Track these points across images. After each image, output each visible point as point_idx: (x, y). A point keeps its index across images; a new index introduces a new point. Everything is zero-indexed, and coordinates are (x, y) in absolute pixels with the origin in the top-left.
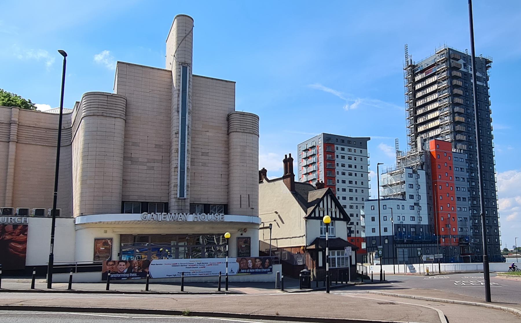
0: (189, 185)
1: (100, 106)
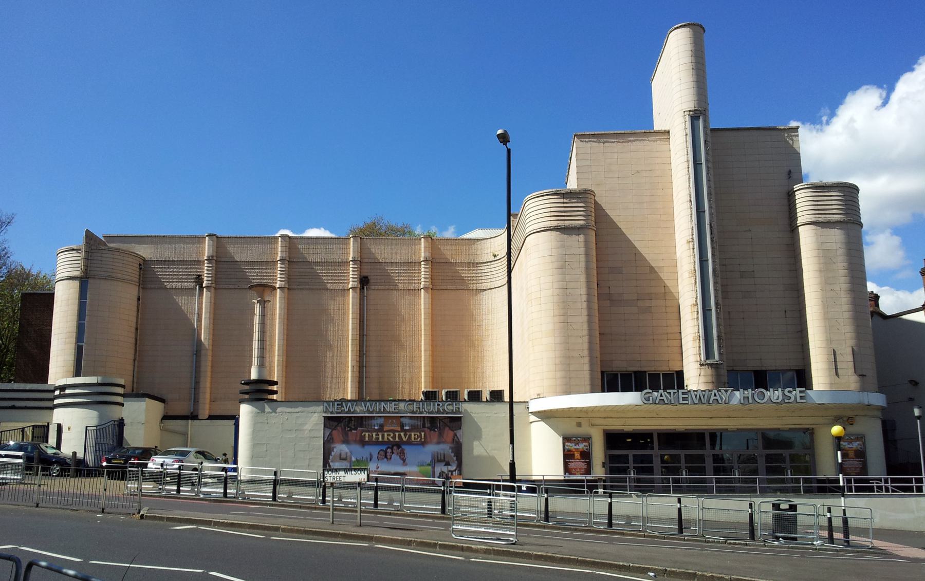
0: (723, 335)
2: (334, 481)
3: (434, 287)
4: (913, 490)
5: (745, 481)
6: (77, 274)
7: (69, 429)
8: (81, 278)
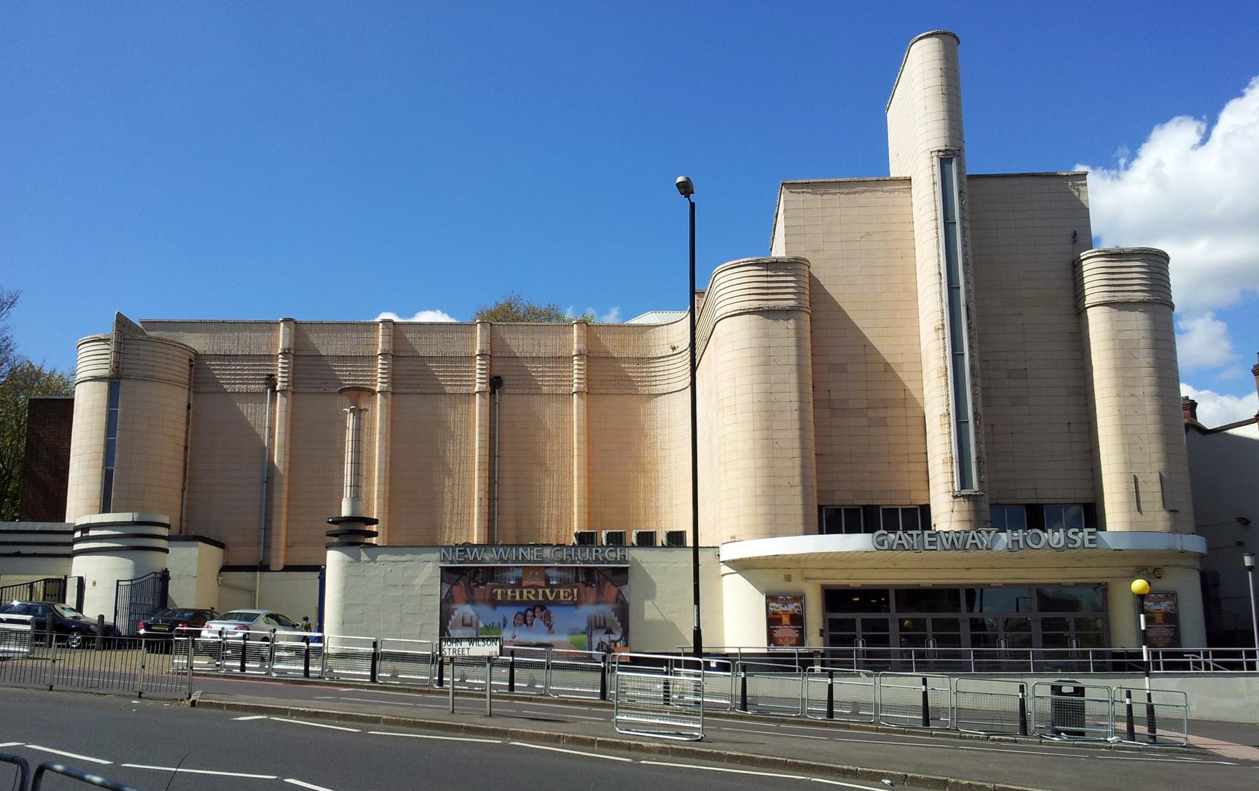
0: (984, 456)
2: (455, 655)
3: (591, 391)
4: (1243, 668)
5: (1014, 655)
6: (105, 372)
7: (94, 584)
8: (110, 378)
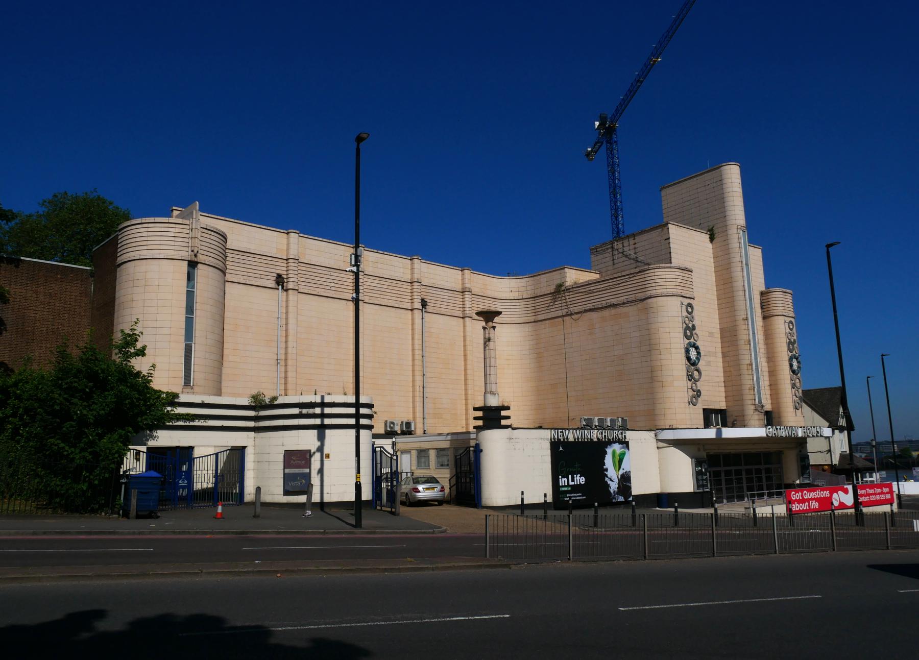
1: (678, 284)
